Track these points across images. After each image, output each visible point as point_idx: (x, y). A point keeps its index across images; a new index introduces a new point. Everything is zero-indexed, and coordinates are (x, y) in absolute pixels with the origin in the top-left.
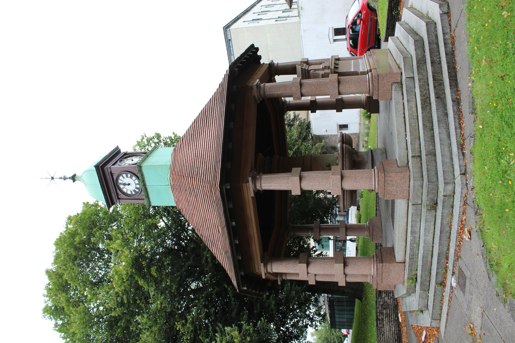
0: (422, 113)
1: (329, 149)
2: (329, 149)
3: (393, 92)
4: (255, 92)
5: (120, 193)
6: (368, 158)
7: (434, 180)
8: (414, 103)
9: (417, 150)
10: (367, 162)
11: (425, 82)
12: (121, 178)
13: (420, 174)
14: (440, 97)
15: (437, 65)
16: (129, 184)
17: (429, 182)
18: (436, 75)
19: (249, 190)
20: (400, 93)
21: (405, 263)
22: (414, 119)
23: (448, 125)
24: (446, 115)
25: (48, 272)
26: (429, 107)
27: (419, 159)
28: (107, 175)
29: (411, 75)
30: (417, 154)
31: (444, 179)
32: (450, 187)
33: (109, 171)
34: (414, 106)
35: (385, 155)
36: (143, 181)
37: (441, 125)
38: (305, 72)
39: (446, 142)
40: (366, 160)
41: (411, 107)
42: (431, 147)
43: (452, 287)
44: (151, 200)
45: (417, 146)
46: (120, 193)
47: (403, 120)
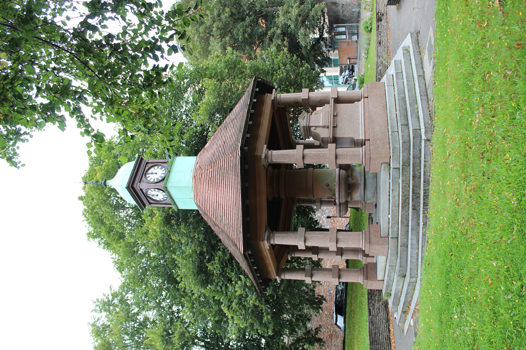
0: (402, 211)
1: (330, 4)
2: (330, 4)
3: (382, 171)
4: (264, 162)
5: (150, 200)
6: (361, 180)
7: (405, 265)
8: (398, 192)
9: (396, 233)
10: (360, 184)
11: (407, 183)
12: (149, 191)
13: (396, 252)
14: (415, 209)
15: (417, 179)
16: (156, 174)
17: (400, 266)
18: (415, 189)
19: (266, 245)
20: (388, 173)
21: (383, 281)
22: (396, 206)
23: (418, 233)
24: (419, 224)
25: (81, 198)
26: (407, 207)
27: (396, 240)
28: (138, 192)
29: (398, 166)
30: (395, 236)
31: (410, 274)
32: (413, 280)
33: (139, 189)
34: (397, 195)
35: (375, 179)
36: (169, 192)
37: (414, 232)
38: (307, 129)
39: (415, 247)
40: (359, 182)
41: (395, 196)
42: (405, 240)
43: (410, 325)
44: (178, 206)
45: (396, 229)
46: (150, 200)
47: (388, 197)
